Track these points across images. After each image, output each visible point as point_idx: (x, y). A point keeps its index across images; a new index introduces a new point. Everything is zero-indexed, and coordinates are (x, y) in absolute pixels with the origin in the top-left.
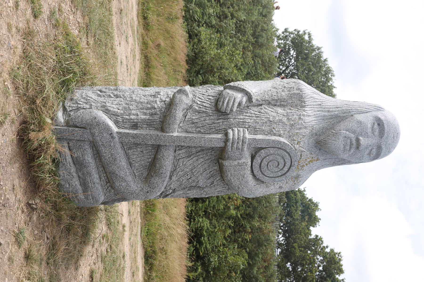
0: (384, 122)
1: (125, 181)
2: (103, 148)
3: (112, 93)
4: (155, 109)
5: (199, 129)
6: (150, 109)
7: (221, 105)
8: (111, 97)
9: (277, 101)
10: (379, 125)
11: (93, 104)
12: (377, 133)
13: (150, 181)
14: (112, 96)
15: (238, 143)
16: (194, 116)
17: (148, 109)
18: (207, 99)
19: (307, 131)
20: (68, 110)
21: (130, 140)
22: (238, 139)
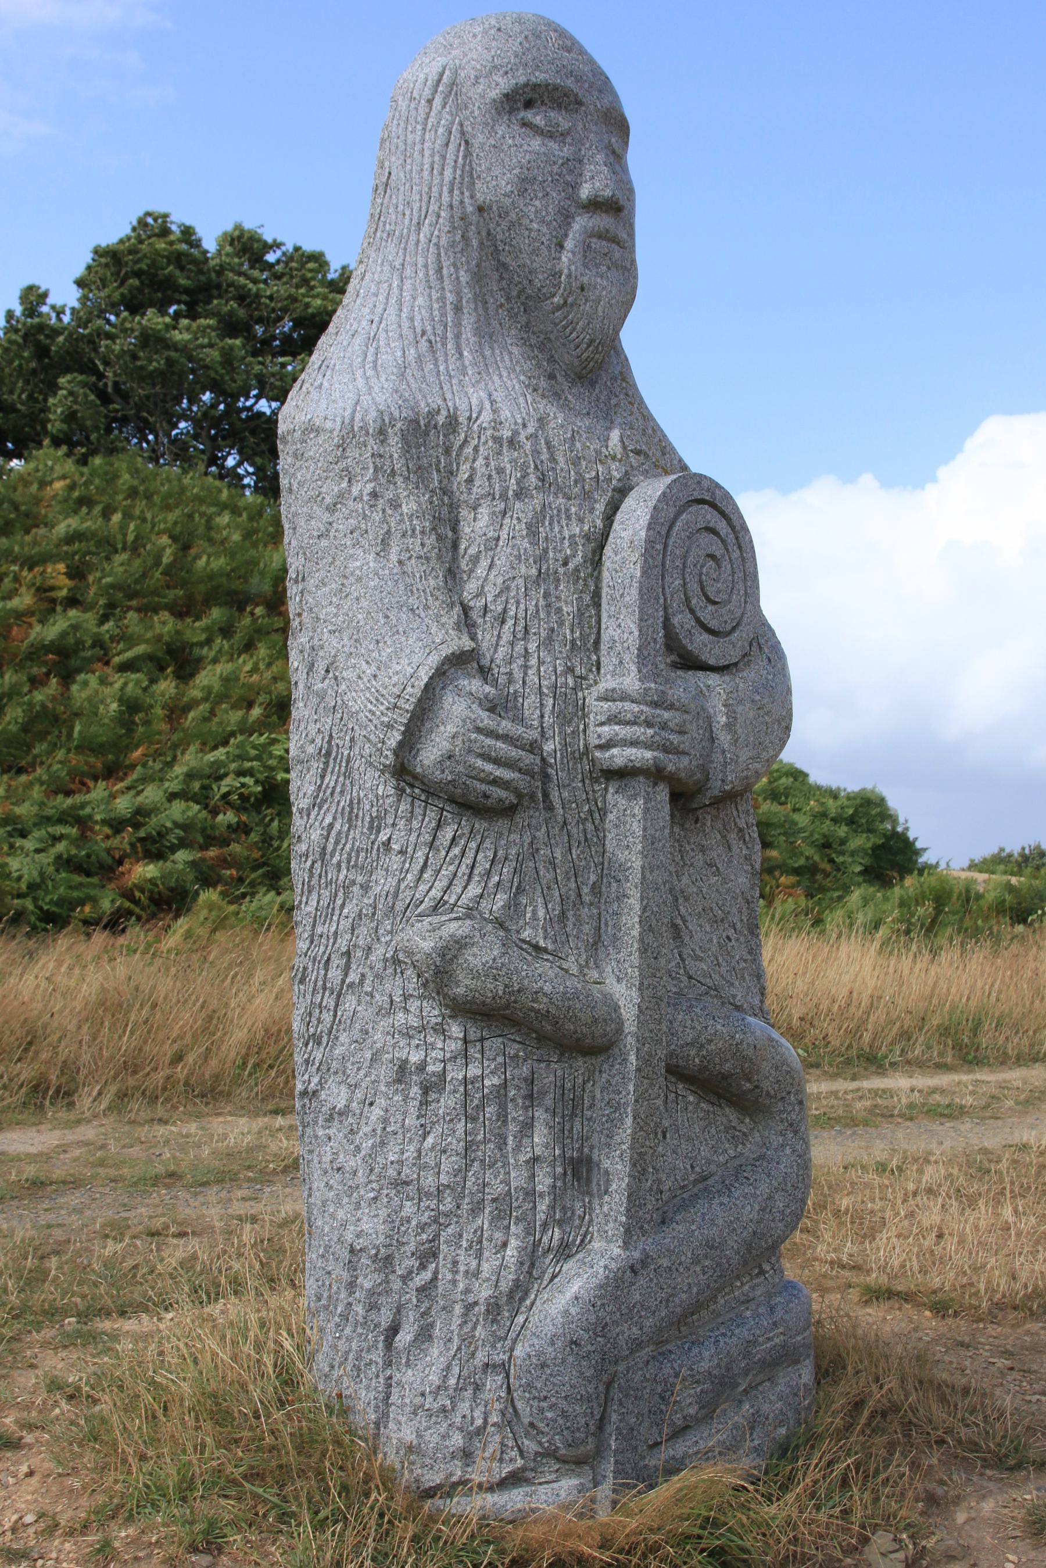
0: (522, 80)
1: (770, 1198)
2: (677, 1300)
3: (405, 1278)
4: (505, 1085)
5: (586, 890)
6: (503, 1106)
7: (503, 794)
8: (435, 1278)
9: (440, 538)
10: (529, 104)
11: (481, 1357)
12: (562, 120)
13: (768, 1094)
14: (427, 1275)
15: (664, 726)
16: (534, 913)
17: (502, 1117)
18: (456, 851)
19: (557, 418)
20: (520, 1463)
21: (651, 1189)
22: (649, 724)
